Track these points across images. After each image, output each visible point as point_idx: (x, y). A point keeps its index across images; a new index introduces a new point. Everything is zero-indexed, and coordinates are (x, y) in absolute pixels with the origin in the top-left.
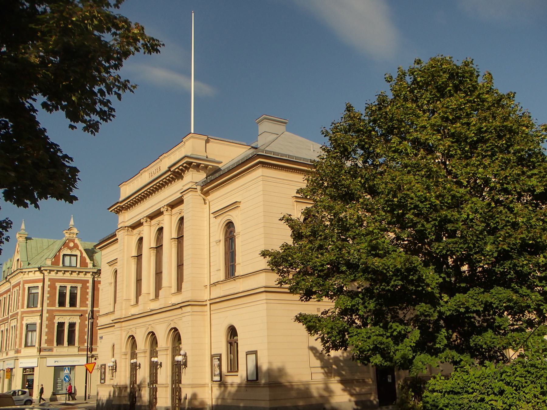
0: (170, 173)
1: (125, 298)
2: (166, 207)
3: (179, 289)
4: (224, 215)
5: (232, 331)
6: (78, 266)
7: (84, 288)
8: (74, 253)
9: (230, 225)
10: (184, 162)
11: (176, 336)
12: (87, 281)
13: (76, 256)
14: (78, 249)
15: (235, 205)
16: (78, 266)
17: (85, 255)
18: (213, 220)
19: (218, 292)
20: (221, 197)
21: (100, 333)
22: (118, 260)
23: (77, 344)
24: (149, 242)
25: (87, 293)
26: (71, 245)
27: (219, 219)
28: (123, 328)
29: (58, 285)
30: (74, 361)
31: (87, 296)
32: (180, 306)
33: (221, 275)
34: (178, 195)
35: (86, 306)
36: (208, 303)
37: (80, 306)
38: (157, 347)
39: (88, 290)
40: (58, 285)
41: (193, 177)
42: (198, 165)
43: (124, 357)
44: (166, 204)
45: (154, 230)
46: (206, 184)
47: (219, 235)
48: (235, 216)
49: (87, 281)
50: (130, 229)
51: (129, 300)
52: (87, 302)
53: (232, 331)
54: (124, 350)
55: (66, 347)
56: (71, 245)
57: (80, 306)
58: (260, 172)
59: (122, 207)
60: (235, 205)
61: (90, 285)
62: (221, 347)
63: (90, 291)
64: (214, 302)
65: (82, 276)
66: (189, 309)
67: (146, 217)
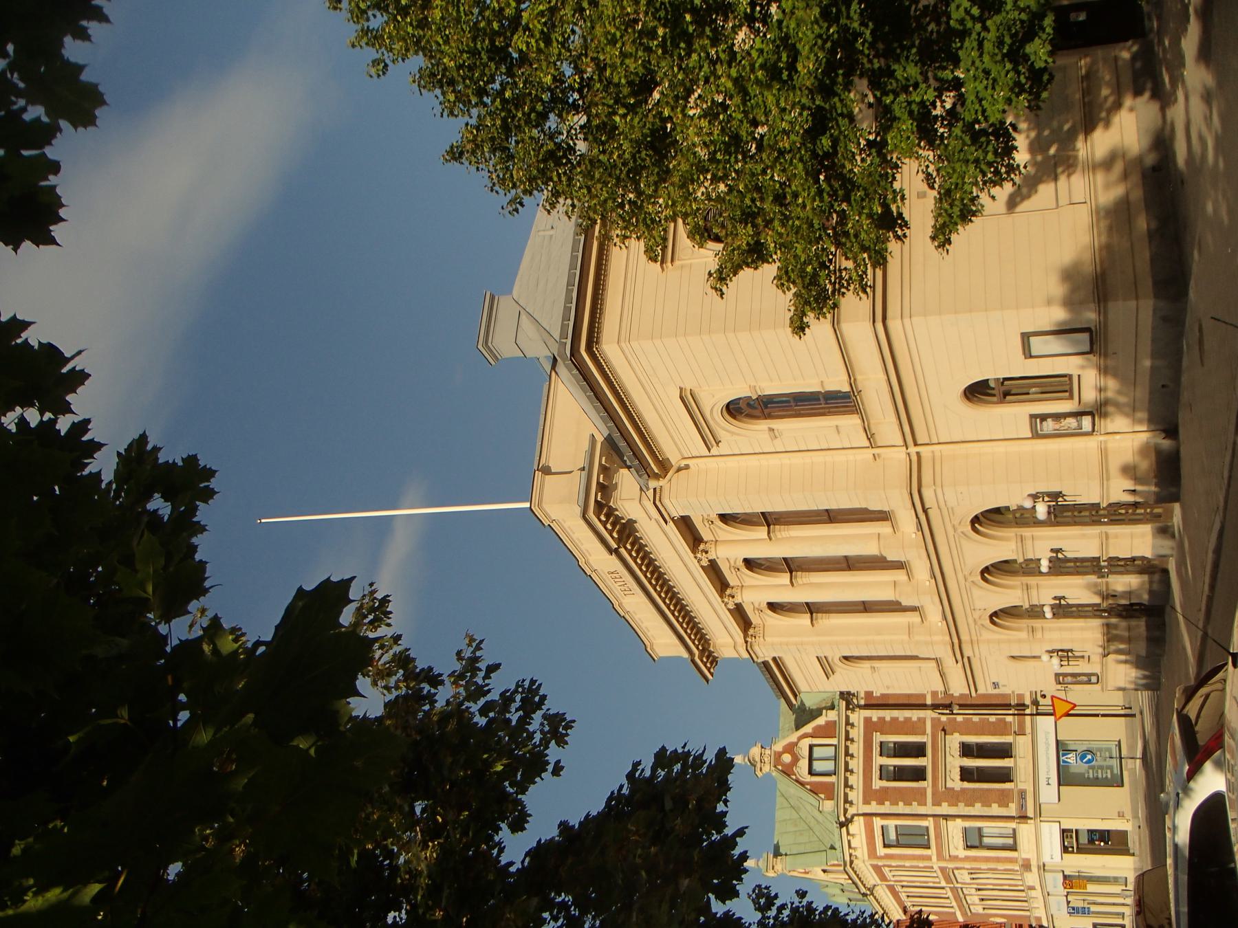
0: (622, 550)
1: (906, 637)
2: (699, 555)
3: (882, 516)
4: (711, 422)
5: (978, 392)
6: (834, 741)
7: (882, 726)
8: (805, 752)
9: (735, 409)
10: (596, 520)
11: (991, 518)
12: (868, 721)
13: (811, 747)
14: (796, 744)
15: (689, 401)
16: (834, 741)
17: (808, 728)
18: (723, 449)
19: (887, 428)
20: (671, 432)
21: (984, 688)
22: (821, 655)
23: (1008, 739)
24: (778, 587)
25: (894, 720)
26: (787, 758)
27: (721, 434)
28: (974, 638)
29: (877, 784)
30: (1047, 744)
31: (901, 719)
32: (923, 512)
33: (850, 422)
34: (671, 528)
35: (922, 721)
36: (913, 450)
37: (924, 733)
38: (1015, 561)
39: (888, 719)
40: (877, 784)
41: (629, 497)
42: (602, 488)
43: (1039, 635)
44: (692, 555)
45: (750, 578)
46: (643, 469)
47: (757, 432)
48: (714, 399)
49: (868, 721)
50: (751, 632)
51: (910, 628)
52: (915, 719)
53: (978, 392)
54: (1023, 635)
55: (1015, 763)
56: (787, 758)
57: (924, 733)
58: (609, 348)
59: (702, 652)
60: (689, 401)
61: (875, 715)
62: (1014, 416)
63: (888, 714)
64: (910, 436)
65: (857, 733)
66: (928, 493)
67: (721, 597)
